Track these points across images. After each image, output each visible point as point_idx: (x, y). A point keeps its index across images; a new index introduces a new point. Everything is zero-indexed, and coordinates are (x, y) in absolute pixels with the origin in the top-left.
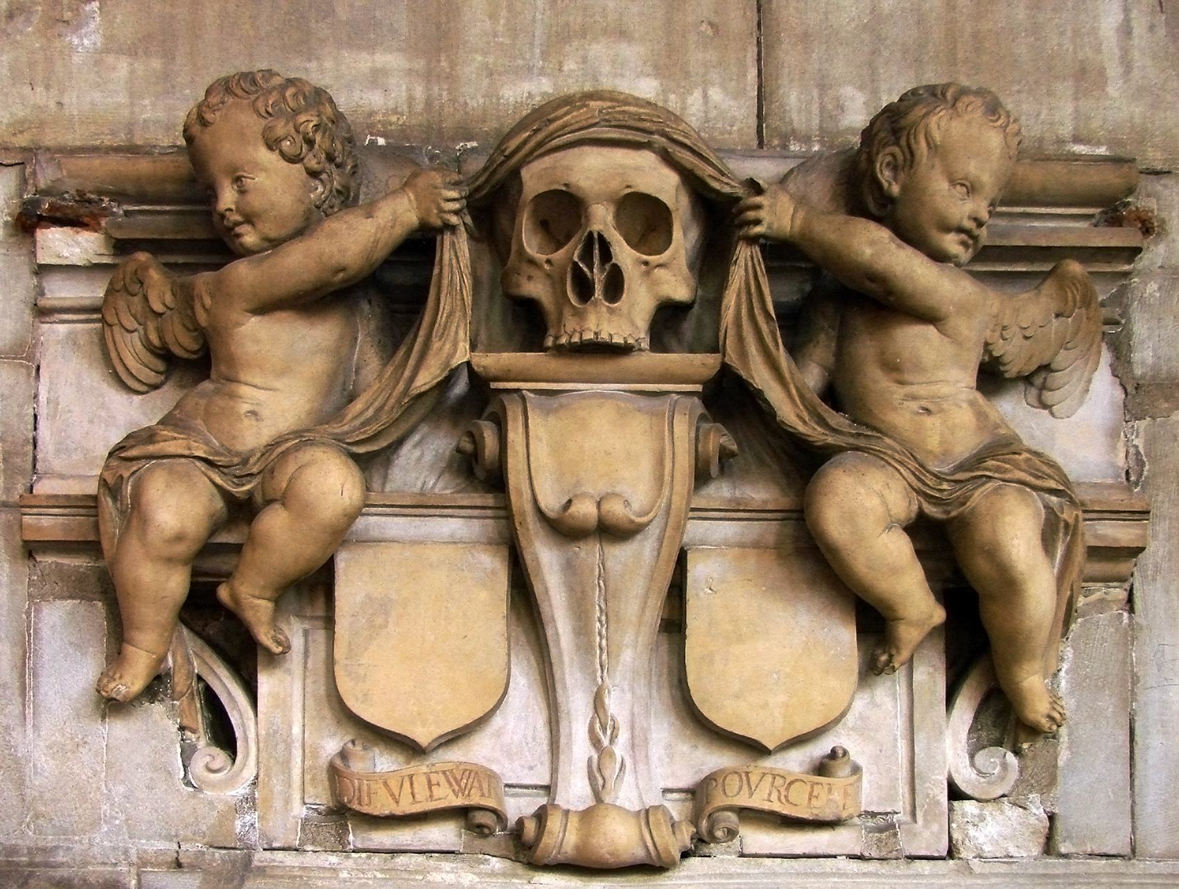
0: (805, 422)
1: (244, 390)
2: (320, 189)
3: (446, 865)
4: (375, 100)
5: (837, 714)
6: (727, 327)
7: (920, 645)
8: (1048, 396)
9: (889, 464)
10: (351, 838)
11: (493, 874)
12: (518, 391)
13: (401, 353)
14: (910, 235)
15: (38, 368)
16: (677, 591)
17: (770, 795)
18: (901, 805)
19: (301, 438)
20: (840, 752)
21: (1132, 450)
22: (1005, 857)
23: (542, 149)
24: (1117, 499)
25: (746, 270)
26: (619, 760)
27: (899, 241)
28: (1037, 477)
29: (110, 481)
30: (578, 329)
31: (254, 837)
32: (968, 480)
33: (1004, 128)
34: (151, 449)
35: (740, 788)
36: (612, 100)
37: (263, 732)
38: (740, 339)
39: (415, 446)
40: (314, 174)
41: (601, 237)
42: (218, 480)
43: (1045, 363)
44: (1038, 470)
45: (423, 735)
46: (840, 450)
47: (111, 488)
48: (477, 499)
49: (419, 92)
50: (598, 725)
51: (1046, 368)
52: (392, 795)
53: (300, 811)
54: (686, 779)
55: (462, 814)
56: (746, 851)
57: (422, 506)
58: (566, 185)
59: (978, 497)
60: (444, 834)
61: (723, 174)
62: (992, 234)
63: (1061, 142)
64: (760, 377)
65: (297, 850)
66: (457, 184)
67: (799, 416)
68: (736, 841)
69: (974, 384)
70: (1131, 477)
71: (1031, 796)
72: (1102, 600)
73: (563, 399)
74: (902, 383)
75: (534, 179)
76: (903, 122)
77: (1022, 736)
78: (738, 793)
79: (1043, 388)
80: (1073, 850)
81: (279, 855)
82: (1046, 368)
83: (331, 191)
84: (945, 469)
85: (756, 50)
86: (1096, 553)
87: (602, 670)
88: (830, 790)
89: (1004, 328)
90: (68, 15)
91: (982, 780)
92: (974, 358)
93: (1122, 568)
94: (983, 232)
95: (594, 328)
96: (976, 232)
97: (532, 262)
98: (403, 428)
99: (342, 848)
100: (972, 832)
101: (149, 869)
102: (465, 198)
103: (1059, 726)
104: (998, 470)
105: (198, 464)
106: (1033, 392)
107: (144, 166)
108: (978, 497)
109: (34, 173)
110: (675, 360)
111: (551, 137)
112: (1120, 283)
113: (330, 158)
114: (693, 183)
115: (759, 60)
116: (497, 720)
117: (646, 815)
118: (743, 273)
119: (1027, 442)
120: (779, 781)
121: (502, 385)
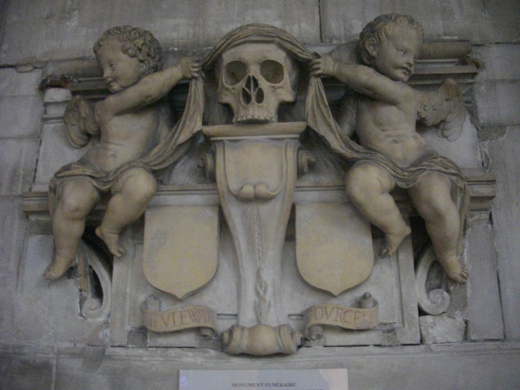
0: (343, 149)
1: (111, 146)
2: (145, 67)
3: (190, 354)
4: (174, 35)
5: (365, 277)
6: (308, 113)
7: (402, 244)
8: (446, 133)
9: (381, 165)
10: (149, 341)
11: (211, 358)
12: (222, 141)
13: (175, 128)
14: (381, 71)
15: (41, 141)
16: (292, 222)
17: (336, 318)
18: (396, 320)
19: (130, 165)
20: (368, 296)
21: (483, 154)
22: (446, 342)
23: (229, 46)
24: (479, 175)
25: (315, 88)
26: (268, 302)
27: (377, 73)
28: (447, 168)
29: (52, 187)
30: (245, 114)
31: (107, 341)
32: (416, 171)
33: (417, 28)
34: (68, 173)
35: (323, 315)
36: (258, 26)
37: (114, 291)
38: (314, 116)
39: (182, 165)
40: (142, 61)
41: (254, 78)
42: (95, 184)
43: (443, 119)
44: (446, 165)
45: (180, 293)
46: (358, 159)
47: (53, 190)
48: (206, 186)
49: (191, 31)
50: (258, 286)
51: (443, 121)
53: (128, 328)
54: (299, 311)
55: (198, 330)
56: (327, 344)
57: (183, 190)
58: (240, 59)
59: (421, 178)
60: (189, 339)
62: (415, 69)
63: (439, 35)
64: (322, 130)
65: (125, 347)
66: (198, 61)
67: (341, 146)
68: (322, 340)
70: (485, 165)
71: (456, 312)
72: (478, 220)
74: (383, 130)
75: (228, 57)
76: (375, 28)
77: (449, 284)
78: (322, 317)
79: (443, 130)
80: (478, 338)
81: (118, 350)
82: (443, 121)
83: (149, 67)
84: (405, 166)
85: (318, 9)
86: (473, 199)
88: (364, 315)
89: (425, 106)
90: (67, 16)
91: (434, 305)
92: (414, 118)
93: (485, 205)
94: (412, 69)
95: (252, 114)
96: (410, 68)
97: (227, 89)
98: (176, 157)
99: (144, 346)
100: (430, 331)
101: (62, 356)
102: (201, 66)
103: (466, 279)
104: (429, 166)
105: (87, 178)
106: (439, 131)
107: (85, 64)
108: (421, 178)
109: (47, 70)
110: (287, 125)
111: (234, 41)
112: (469, 87)
113: (149, 55)
114: (291, 55)
115: (320, 12)
116: (215, 284)
117: (278, 329)
118: (314, 89)
119: (440, 153)
120: (340, 311)
121: (215, 139)
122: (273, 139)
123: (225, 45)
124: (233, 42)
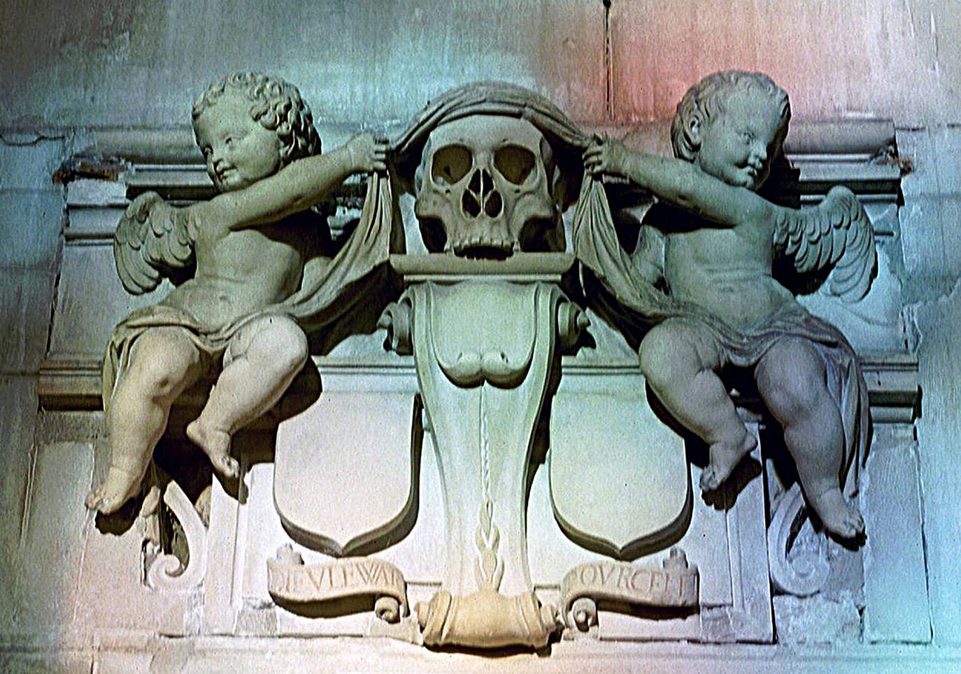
42: (198, 342)
52: (315, 583)
61: (574, 132)
63: (838, 110)
65: (232, 636)
69: (769, 271)
73: (457, 286)
87: (487, 488)
90: (106, 41)
111: (451, 110)
114: (548, 135)
121: (412, 278)
122: (515, 282)
123: (437, 115)
124: (451, 112)
